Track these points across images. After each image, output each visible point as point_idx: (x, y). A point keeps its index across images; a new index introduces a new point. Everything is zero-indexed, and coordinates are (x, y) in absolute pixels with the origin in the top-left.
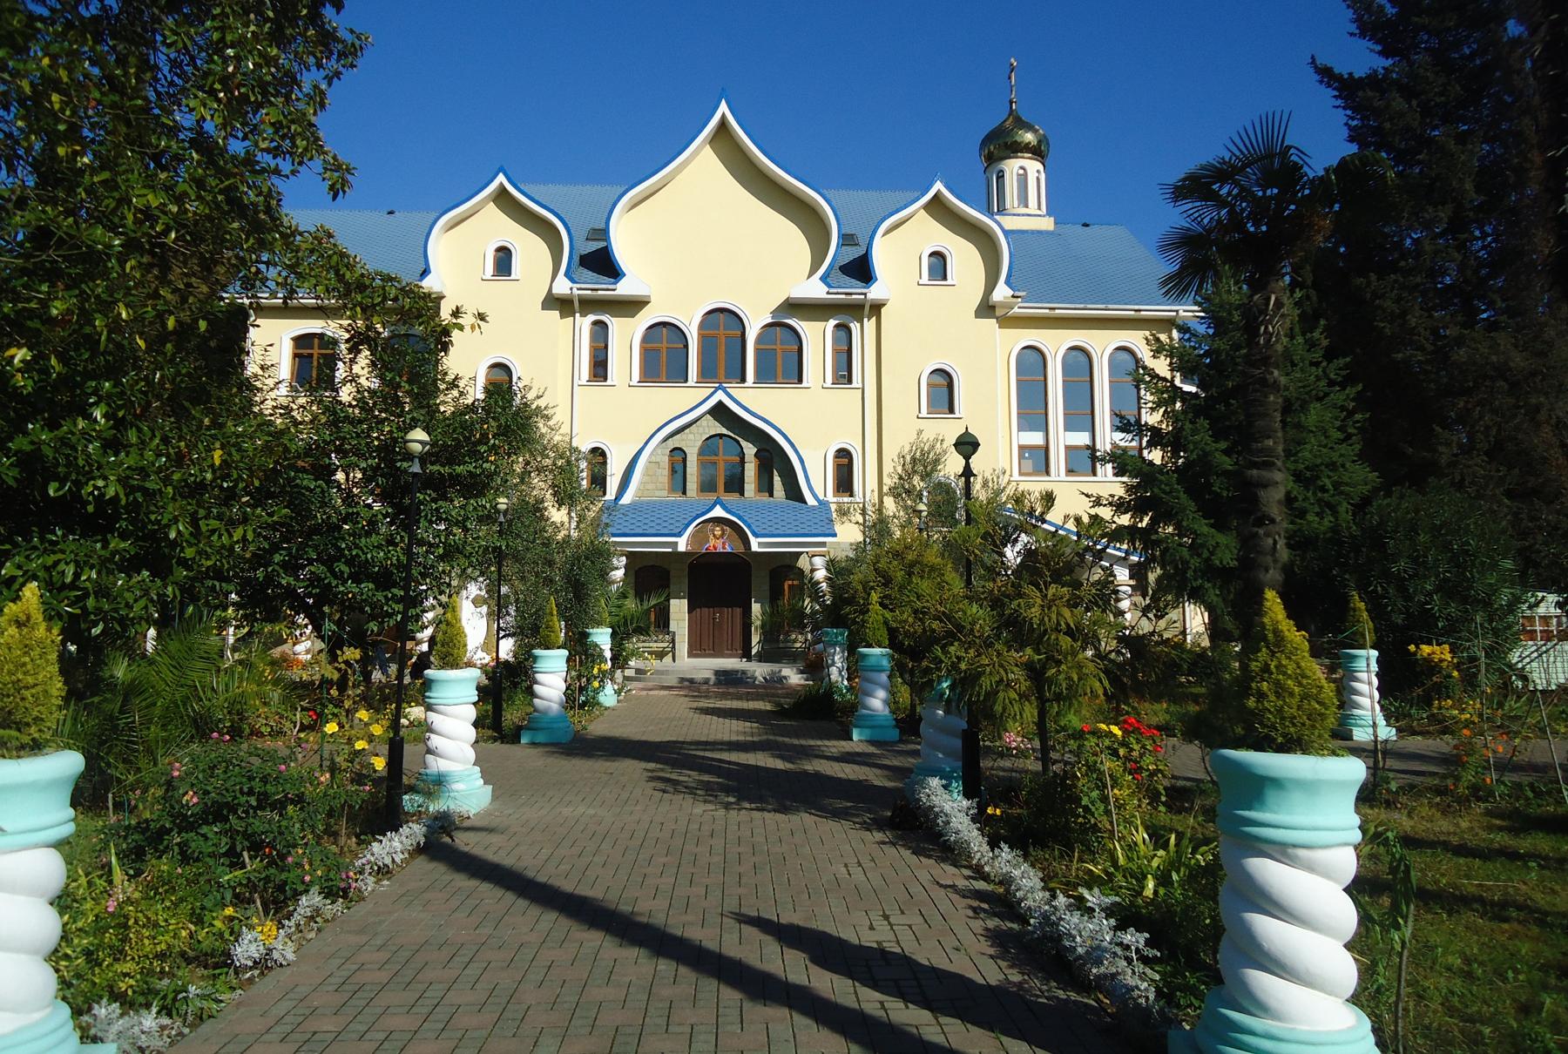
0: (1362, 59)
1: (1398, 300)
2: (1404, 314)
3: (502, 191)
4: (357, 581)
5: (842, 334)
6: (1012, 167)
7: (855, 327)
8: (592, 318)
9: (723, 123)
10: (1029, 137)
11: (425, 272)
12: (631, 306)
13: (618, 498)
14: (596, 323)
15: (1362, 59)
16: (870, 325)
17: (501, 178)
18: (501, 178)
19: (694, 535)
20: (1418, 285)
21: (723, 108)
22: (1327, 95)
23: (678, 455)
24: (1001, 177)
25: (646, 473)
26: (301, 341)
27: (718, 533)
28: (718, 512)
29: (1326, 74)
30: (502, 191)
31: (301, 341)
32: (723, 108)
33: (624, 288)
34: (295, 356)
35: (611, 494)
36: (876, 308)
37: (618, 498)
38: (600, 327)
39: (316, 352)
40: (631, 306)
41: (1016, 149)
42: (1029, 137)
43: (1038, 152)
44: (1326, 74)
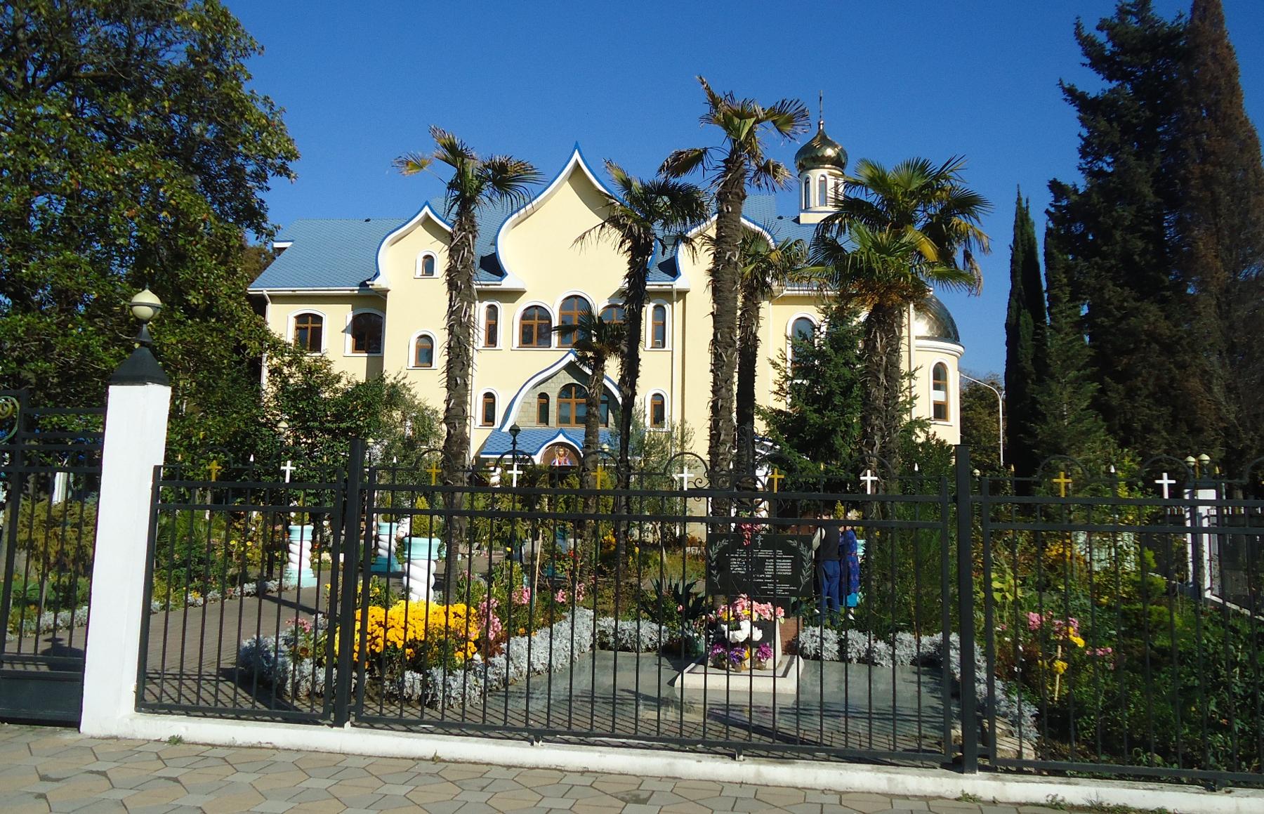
0: (1095, 85)
1: (1097, 277)
2: (1102, 289)
3: (427, 218)
4: (1125, 54)
5: (659, 312)
6: (816, 175)
7: (668, 307)
8: (486, 303)
9: (577, 165)
10: (830, 152)
11: (377, 275)
12: (512, 295)
13: (502, 426)
14: (490, 307)
15: (1095, 85)
16: (678, 306)
17: (426, 209)
18: (426, 209)
19: (546, 454)
20: (1113, 266)
21: (577, 156)
22: (1072, 112)
23: (543, 396)
24: (807, 183)
25: (522, 410)
26: (301, 318)
27: (562, 452)
28: (561, 439)
29: (1073, 95)
30: (427, 218)
31: (301, 318)
32: (577, 156)
33: (506, 284)
34: (297, 328)
35: (497, 426)
36: (682, 294)
37: (502, 426)
38: (493, 312)
39: (310, 325)
40: (512, 295)
41: (820, 161)
42: (830, 152)
43: (838, 162)
44: (1073, 95)
